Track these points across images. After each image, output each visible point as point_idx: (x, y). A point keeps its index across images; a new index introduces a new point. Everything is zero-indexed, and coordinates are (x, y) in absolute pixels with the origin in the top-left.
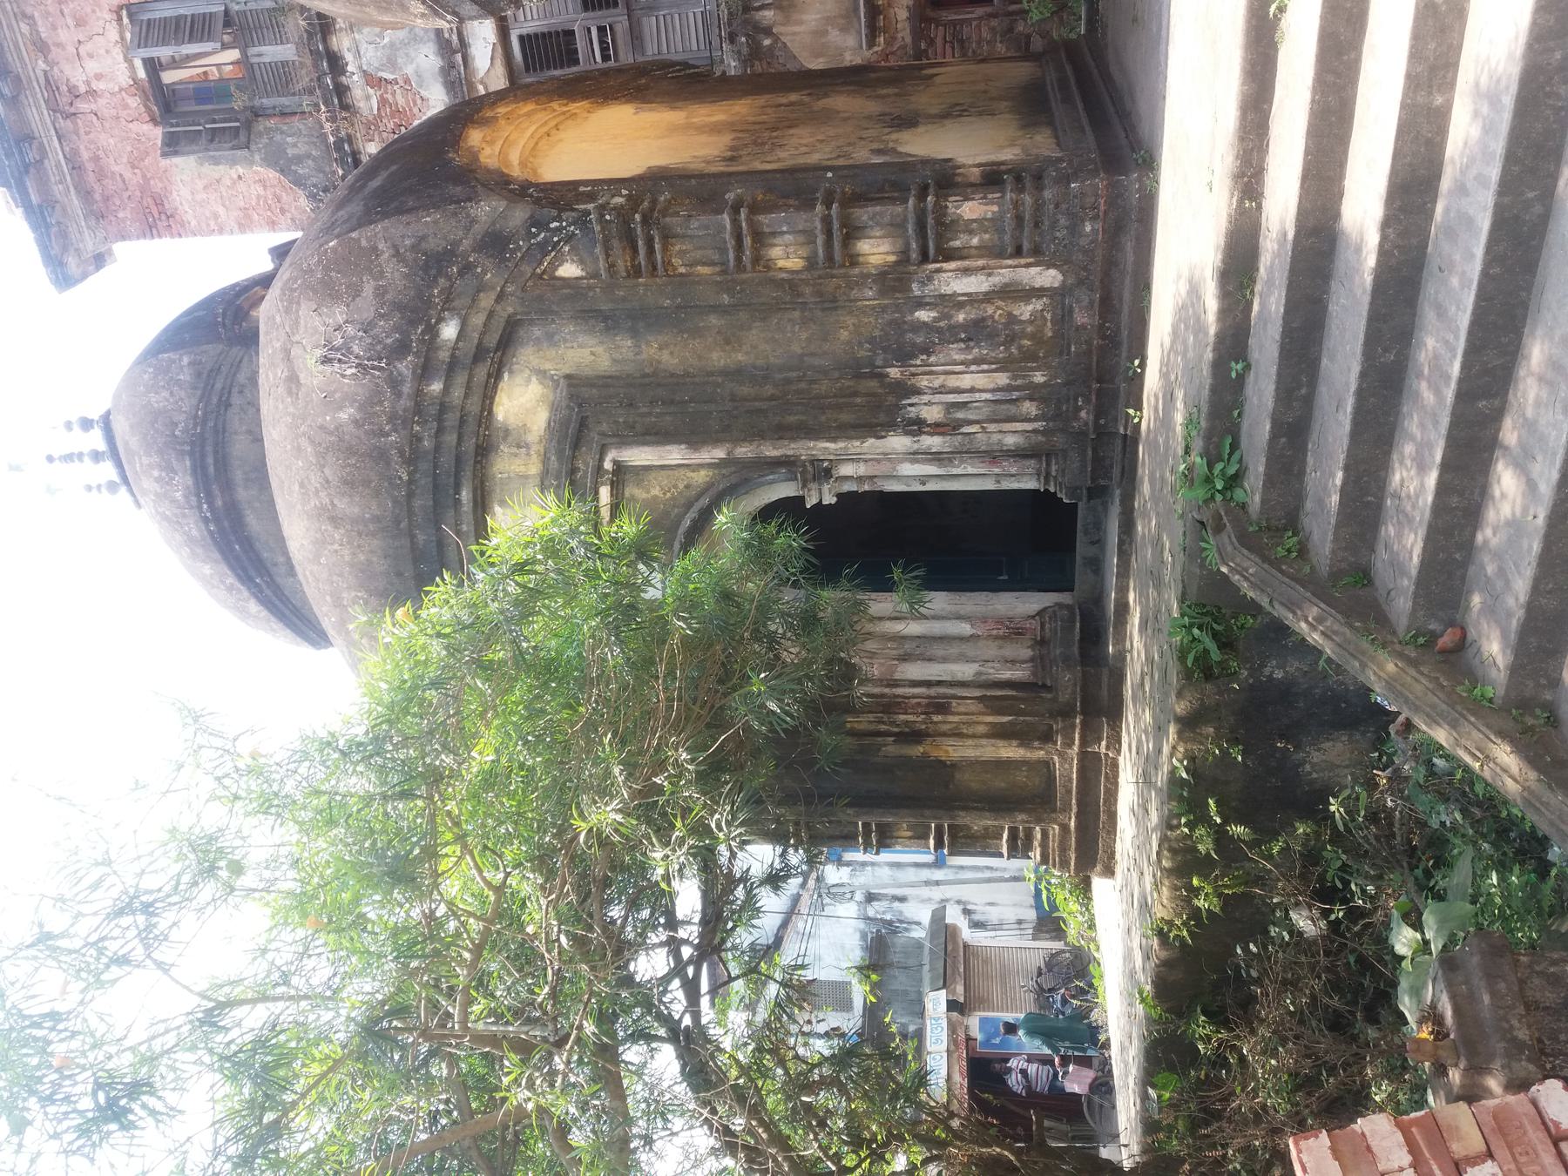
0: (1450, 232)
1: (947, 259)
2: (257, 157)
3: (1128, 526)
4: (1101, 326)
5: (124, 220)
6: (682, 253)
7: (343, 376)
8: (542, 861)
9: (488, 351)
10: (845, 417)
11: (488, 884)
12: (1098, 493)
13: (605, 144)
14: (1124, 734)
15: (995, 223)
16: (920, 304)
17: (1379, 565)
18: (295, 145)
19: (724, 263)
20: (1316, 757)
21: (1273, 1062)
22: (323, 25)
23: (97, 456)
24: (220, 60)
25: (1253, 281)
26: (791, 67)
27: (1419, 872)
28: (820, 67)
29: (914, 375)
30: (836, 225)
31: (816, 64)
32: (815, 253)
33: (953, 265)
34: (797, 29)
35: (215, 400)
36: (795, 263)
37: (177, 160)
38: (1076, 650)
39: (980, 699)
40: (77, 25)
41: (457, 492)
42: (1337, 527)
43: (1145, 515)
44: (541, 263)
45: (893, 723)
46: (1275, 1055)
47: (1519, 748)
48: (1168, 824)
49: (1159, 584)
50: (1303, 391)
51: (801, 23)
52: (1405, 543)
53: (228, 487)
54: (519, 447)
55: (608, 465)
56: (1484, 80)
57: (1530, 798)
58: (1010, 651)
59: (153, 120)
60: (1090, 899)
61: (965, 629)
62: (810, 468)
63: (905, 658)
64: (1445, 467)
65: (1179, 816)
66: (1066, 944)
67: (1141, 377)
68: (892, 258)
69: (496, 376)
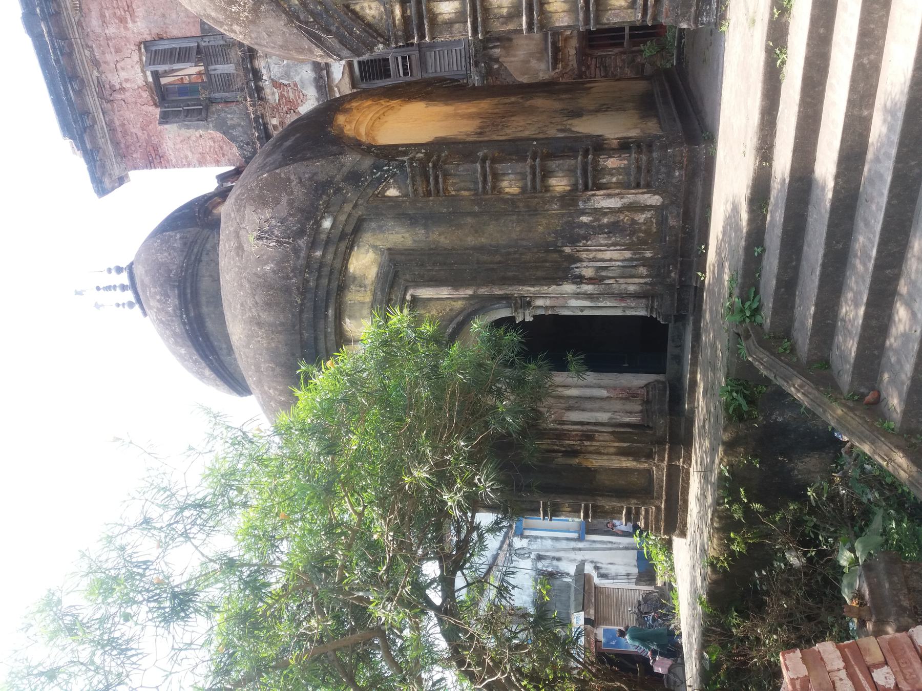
0: (871, 181)
1: (599, 189)
2: (211, 125)
3: (697, 337)
4: (683, 227)
5: (136, 159)
6: (454, 184)
7: (268, 247)
8: (382, 501)
9: (347, 235)
10: (539, 273)
11: (355, 511)
12: (680, 318)
13: (410, 124)
14: (693, 454)
15: (626, 170)
16: (583, 213)
17: (834, 357)
18: (232, 119)
19: (476, 189)
20: (801, 466)
21: (775, 637)
22: (251, 54)
23: (123, 288)
24: (190, 71)
25: (767, 204)
26: (509, 80)
27: (856, 529)
28: (525, 81)
29: (578, 251)
30: (538, 170)
31: (524, 79)
32: (526, 184)
33: (602, 192)
34: (513, 59)
35: (193, 258)
36: (514, 190)
37: (167, 126)
38: (666, 407)
39: (612, 433)
40: (116, 52)
41: (327, 311)
42: (812, 336)
43: (707, 331)
44: (377, 188)
45: (561, 445)
46: (776, 632)
47: (907, 455)
48: (718, 502)
49: (714, 369)
50: (794, 264)
51: (515, 56)
52: (848, 346)
53: (197, 305)
54: (361, 286)
55: (408, 297)
56: (889, 104)
57: (913, 482)
58: (630, 406)
59: (155, 105)
60: (671, 553)
61: (604, 393)
62: (519, 301)
63: (569, 409)
64: (868, 305)
65: (723, 498)
66: (656, 587)
67: (705, 255)
68: (568, 188)
69: (350, 248)
